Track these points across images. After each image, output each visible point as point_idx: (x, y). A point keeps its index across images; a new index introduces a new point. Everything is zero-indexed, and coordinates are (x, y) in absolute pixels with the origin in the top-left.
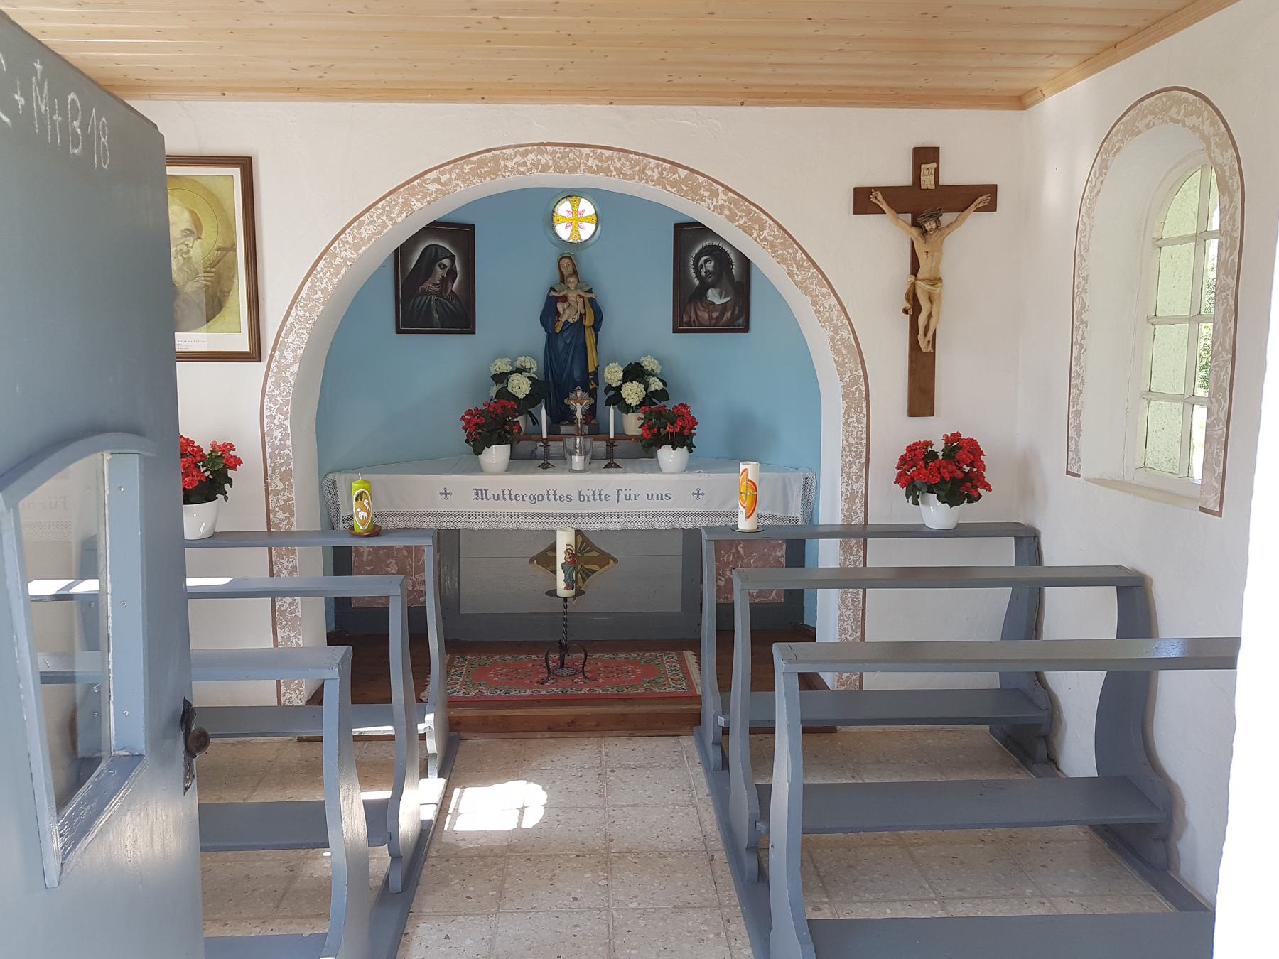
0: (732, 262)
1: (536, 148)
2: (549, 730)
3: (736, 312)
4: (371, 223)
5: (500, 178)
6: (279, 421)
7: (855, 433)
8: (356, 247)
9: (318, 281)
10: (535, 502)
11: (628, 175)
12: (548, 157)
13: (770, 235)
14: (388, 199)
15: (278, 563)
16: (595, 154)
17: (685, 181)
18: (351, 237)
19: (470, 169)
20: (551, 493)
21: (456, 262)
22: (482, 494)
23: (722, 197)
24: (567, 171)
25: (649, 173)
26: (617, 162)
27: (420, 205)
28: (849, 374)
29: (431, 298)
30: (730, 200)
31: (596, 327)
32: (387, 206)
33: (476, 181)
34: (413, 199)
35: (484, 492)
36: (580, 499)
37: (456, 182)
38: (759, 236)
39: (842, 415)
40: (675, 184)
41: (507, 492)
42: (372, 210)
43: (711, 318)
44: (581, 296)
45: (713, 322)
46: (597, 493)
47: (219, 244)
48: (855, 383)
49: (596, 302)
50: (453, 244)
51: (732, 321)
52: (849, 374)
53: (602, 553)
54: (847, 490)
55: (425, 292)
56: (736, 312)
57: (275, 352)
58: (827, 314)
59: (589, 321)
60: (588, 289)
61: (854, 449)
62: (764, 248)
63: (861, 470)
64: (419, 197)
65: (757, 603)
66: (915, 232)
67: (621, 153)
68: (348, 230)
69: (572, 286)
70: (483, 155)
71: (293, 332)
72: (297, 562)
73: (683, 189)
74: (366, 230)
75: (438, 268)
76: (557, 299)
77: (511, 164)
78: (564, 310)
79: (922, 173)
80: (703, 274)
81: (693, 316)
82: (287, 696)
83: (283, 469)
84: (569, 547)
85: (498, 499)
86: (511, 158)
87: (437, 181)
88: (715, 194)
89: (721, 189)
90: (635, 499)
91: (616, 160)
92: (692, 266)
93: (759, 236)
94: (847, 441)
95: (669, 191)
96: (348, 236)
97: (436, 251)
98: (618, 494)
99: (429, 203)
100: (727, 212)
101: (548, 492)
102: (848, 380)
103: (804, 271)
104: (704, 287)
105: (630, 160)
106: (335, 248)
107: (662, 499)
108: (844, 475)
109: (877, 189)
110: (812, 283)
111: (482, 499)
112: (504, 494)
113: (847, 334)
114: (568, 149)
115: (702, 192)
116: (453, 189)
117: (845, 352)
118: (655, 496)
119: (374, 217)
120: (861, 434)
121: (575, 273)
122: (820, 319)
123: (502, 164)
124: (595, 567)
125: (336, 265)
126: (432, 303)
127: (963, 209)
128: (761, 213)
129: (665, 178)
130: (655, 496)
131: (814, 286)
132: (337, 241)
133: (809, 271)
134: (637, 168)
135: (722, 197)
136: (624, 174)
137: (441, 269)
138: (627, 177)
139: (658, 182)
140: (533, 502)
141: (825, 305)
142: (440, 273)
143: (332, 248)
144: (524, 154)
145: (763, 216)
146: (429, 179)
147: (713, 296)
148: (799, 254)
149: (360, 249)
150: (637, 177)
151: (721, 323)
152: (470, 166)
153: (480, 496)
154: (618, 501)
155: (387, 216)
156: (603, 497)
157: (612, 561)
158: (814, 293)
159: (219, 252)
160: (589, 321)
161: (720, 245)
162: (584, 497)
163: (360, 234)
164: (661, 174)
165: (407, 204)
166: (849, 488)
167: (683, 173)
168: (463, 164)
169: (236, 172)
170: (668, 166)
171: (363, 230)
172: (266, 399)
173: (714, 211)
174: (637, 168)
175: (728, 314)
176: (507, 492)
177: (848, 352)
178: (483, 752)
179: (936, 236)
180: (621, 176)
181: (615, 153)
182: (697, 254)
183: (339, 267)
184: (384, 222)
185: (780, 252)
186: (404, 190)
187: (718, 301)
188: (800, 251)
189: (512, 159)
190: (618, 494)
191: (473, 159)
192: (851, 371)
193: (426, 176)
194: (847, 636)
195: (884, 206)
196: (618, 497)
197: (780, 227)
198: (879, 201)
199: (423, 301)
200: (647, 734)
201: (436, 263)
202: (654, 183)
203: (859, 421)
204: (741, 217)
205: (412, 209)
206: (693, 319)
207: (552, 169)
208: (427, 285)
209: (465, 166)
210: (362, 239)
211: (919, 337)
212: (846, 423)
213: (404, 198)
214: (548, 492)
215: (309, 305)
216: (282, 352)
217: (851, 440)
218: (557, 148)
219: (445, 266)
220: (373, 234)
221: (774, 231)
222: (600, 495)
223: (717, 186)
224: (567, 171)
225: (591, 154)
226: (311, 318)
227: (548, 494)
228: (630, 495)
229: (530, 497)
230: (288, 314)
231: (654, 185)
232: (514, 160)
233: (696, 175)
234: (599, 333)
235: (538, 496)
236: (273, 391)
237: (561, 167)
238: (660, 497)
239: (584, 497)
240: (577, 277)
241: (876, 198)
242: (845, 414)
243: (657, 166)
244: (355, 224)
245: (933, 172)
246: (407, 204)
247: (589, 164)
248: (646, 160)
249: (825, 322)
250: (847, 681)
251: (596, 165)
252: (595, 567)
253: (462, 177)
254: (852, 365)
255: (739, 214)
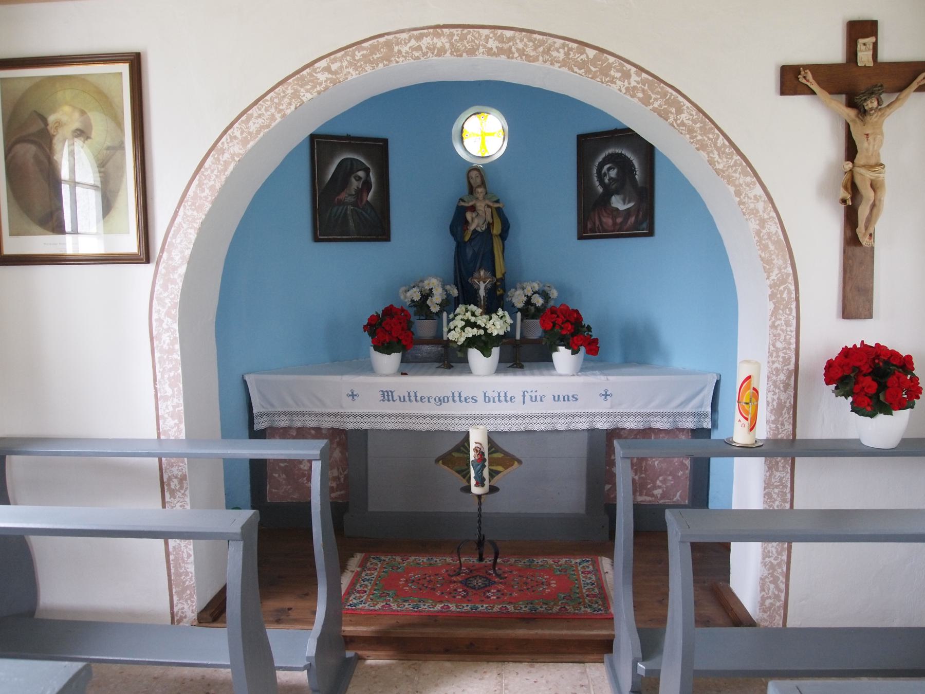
0: (635, 169)
1: (432, 30)
2: (447, 651)
3: (640, 216)
4: (260, 116)
5: (394, 64)
6: (167, 325)
7: (782, 337)
8: (245, 142)
9: (205, 179)
10: (441, 404)
11: (531, 56)
12: (444, 40)
13: (689, 119)
14: (277, 90)
15: (168, 471)
16: (495, 35)
17: (593, 61)
18: (239, 131)
19: (362, 55)
20: (457, 395)
21: (371, 174)
22: (388, 395)
23: (634, 78)
24: (465, 54)
25: (554, 54)
26: (519, 43)
27: (309, 96)
28: (776, 271)
29: (347, 207)
30: (644, 82)
31: (504, 235)
32: (276, 97)
33: (368, 68)
34: (302, 90)
35: (390, 394)
36: (485, 400)
37: (347, 70)
38: (676, 120)
39: (769, 317)
40: (582, 65)
41: (412, 394)
42: (261, 102)
43: (615, 224)
44: (489, 206)
45: (617, 227)
46: (502, 395)
47: (108, 144)
48: (783, 281)
49: (503, 212)
50: (367, 157)
51: (636, 226)
52: (776, 271)
53: (506, 454)
54: (773, 400)
55: (341, 203)
56: (640, 216)
57: (163, 254)
58: (752, 206)
59: (497, 230)
60: (495, 199)
61: (781, 354)
62: (681, 133)
63: (789, 378)
64: (309, 87)
65: (660, 505)
66: (851, 113)
67: (523, 33)
68: (237, 125)
69: (481, 196)
70: (376, 40)
71: (181, 232)
72: (186, 470)
73: (591, 71)
74: (254, 123)
75: (353, 180)
76: (466, 209)
77: (405, 49)
78: (473, 219)
79: (858, 49)
80: (606, 181)
81: (597, 223)
82: (180, 606)
83: (172, 374)
84: (477, 445)
85: (404, 400)
86: (405, 43)
87: (327, 69)
88: (626, 76)
89: (633, 69)
90: (541, 400)
91: (518, 41)
92: (596, 175)
93: (676, 120)
94: (774, 346)
95: (576, 73)
96: (236, 131)
97: (352, 164)
98: (524, 396)
99: (319, 93)
100: (640, 95)
101: (453, 393)
102: (776, 278)
103: (727, 158)
104: (608, 194)
105: (533, 41)
106: (223, 143)
107: (568, 400)
108: (771, 383)
109: (806, 67)
110: (735, 171)
111: (389, 400)
112: (409, 396)
113: (774, 228)
114: (466, 31)
115: (612, 73)
116: (343, 77)
117: (772, 247)
118: (561, 398)
119: (263, 110)
120: (790, 339)
121: (483, 184)
122: (744, 210)
123: (396, 49)
124: (500, 468)
125: (225, 162)
126: (348, 212)
127: (901, 89)
128: (679, 96)
129: (572, 58)
130: (561, 398)
131: (737, 175)
132: (225, 137)
133: (732, 158)
134: (541, 49)
135: (634, 78)
136: (526, 55)
137: (357, 180)
138: (529, 59)
139: (564, 64)
140: (438, 404)
141: (750, 195)
142: (355, 184)
143: (220, 144)
144: (419, 38)
145: (681, 99)
146: (319, 68)
147: (617, 203)
148: (721, 140)
149: (249, 144)
150: (541, 58)
151: (625, 228)
152: (362, 53)
153: (386, 397)
154: (524, 403)
155: (276, 108)
156: (508, 399)
157: (516, 463)
158: (737, 183)
159: (108, 152)
160: (497, 230)
161: (623, 152)
162: (489, 398)
163: (247, 128)
164: (567, 54)
165: (296, 95)
166: (775, 397)
167: (591, 53)
168: (354, 52)
169: (124, 69)
170: (575, 45)
171: (251, 124)
172: (155, 302)
173: (625, 93)
174: (541, 49)
175: (632, 219)
176: (412, 394)
177: (776, 248)
178: (374, 677)
179: (876, 117)
180: (524, 57)
181: (517, 34)
182: (600, 163)
183: (226, 164)
184: (273, 115)
185: (699, 137)
186: (293, 80)
187: (622, 207)
188: (721, 137)
189: (406, 44)
190: (524, 396)
191: (364, 45)
192: (780, 269)
193: (317, 65)
194: (772, 559)
195: (815, 87)
196: (524, 398)
197: (700, 110)
198: (808, 81)
199: (339, 211)
200: (552, 660)
201: (350, 176)
202: (559, 65)
203: (788, 324)
204: (656, 100)
205: (302, 100)
206: (597, 226)
207: (448, 52)
208: (342, 196)
209: (357, 53)
210: (250, 133)
211: (858, 230)
212: (773, 326)
213: (294, 89)
214: (453, 393)
215: (197, 204)
216: (170, 253)
217: (779, 345)
218: (454, 30)
219: (360, 178)
220: (262, 127)
221: (692, 115)
222: (505, 396)
223: (629, 67)
224: (465, 54)
225: (491, 35)
226: (199, 217)
227: (453, 396)
228: (536, 396)
229: (435, 399)
230: (176, 213)
231: (560, 67)
232: (409, 45)
233: (605, 55)
234: (506, 242)
235: (444, 398)
236: (161, 294)
237: (458, 50)
238: (566, 398)
239: (489, 398)
240: (485, 187)
241: (805, 77)
242: (772, 315)
243: (563, 46)
244: (244, 118)
245: (871, 47)
246: (296, 95)
247: (489, 45)
248: (551, 40)
249: (750, 214)
250: (770, 608)
251: (496, 47)
252: (500, 468)
253: (354, 64)
254: (781, 262)
255: (653, 96)
